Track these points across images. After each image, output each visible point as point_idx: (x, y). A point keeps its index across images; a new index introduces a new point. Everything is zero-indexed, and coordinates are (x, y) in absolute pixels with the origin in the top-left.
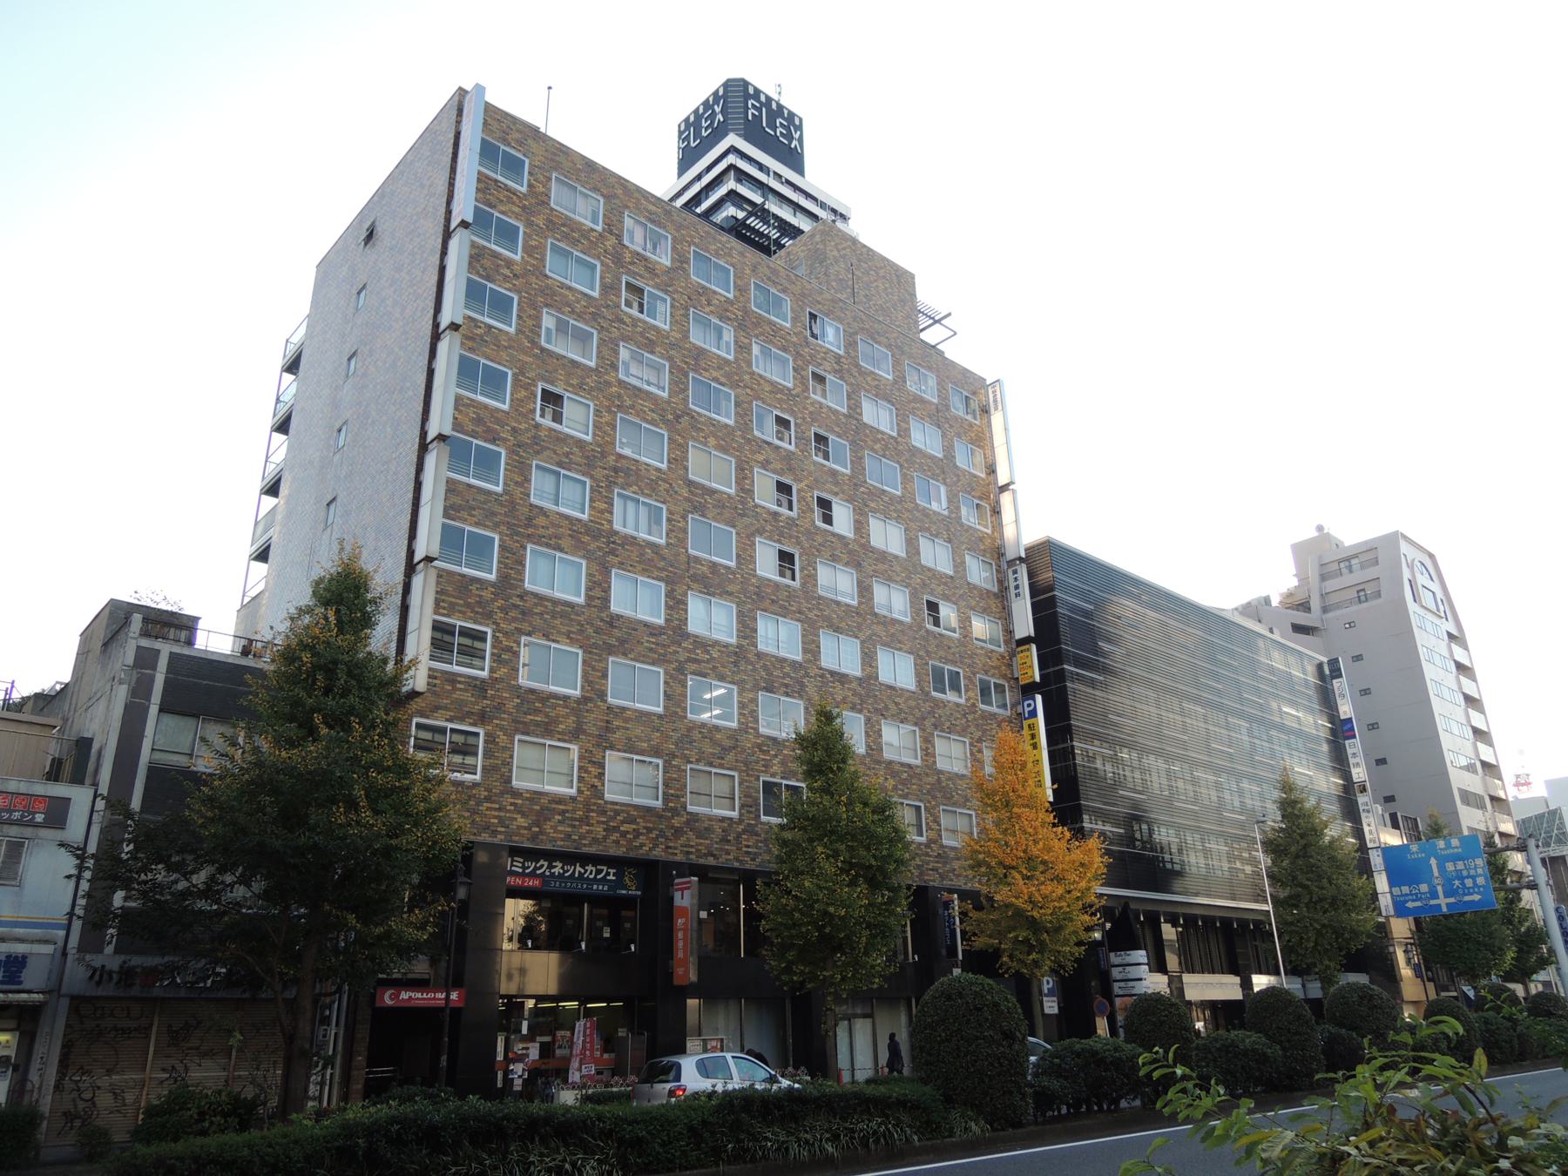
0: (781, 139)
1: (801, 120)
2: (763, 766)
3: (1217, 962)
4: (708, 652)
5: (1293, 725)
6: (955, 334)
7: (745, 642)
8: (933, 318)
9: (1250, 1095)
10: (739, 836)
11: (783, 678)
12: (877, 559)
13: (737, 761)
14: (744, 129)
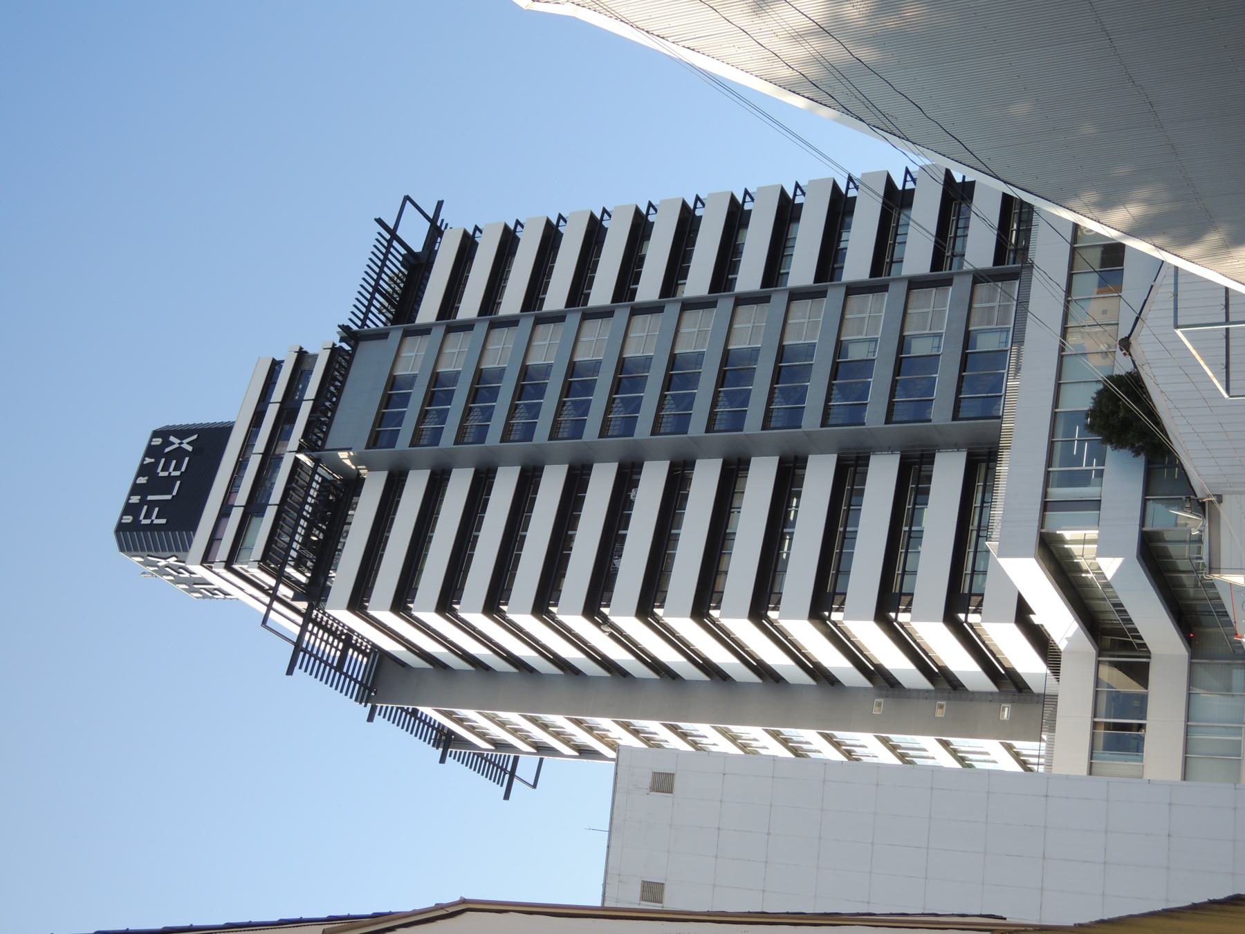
0: (183, 469)
1: (156, 434)
5: (655, 342)
6: (407, 198)
9: (1103, 437)
14: (180, 530)
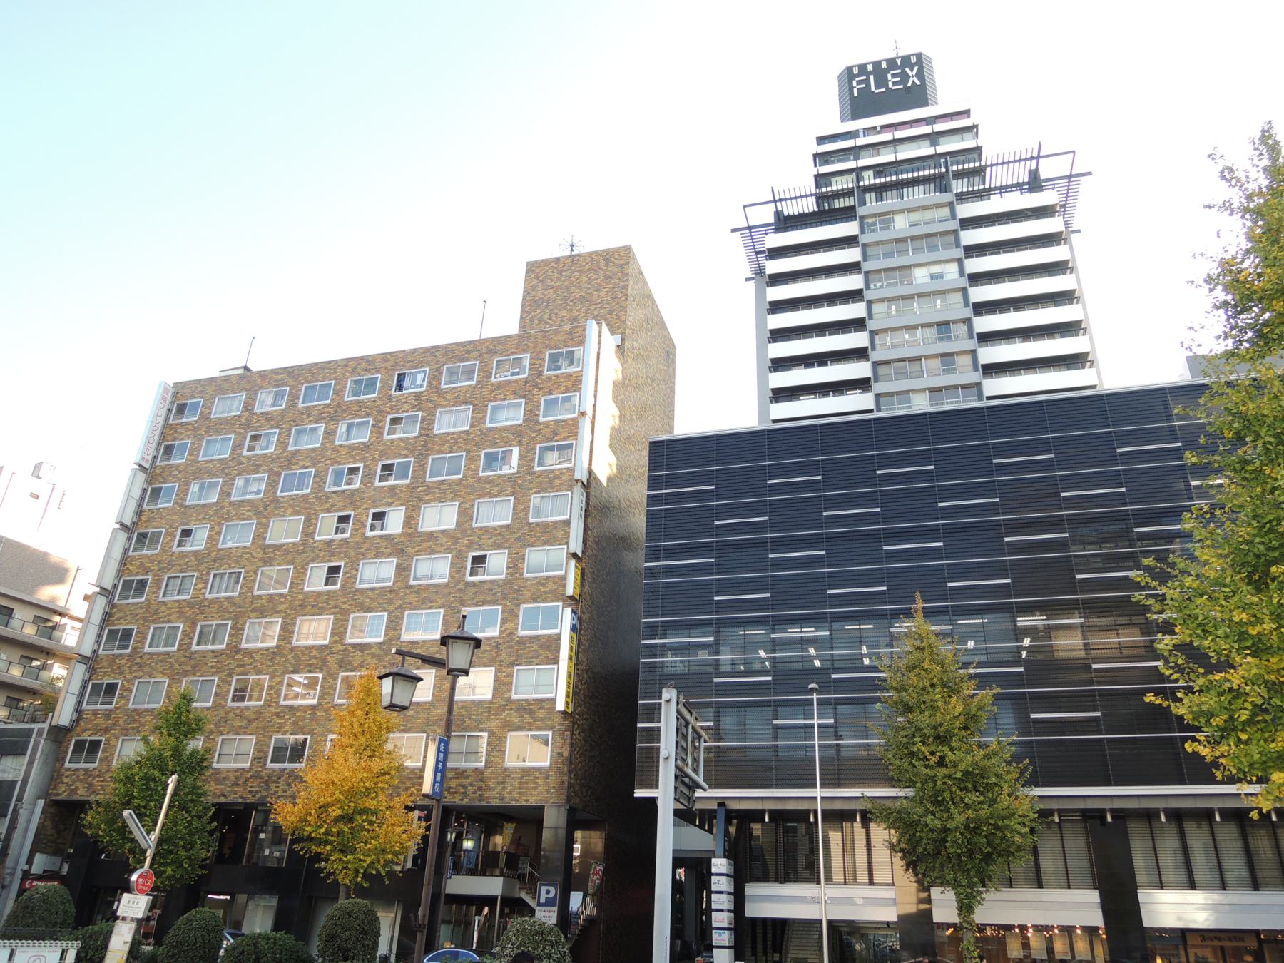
2: (278, 728)
3: (1230, 878)
4: (252, 657)
7: (282, 643)
8: (1032, 158)
10: (247, 780)
11: (310, 660)
12: (421, 541)
13: (257, 728)
